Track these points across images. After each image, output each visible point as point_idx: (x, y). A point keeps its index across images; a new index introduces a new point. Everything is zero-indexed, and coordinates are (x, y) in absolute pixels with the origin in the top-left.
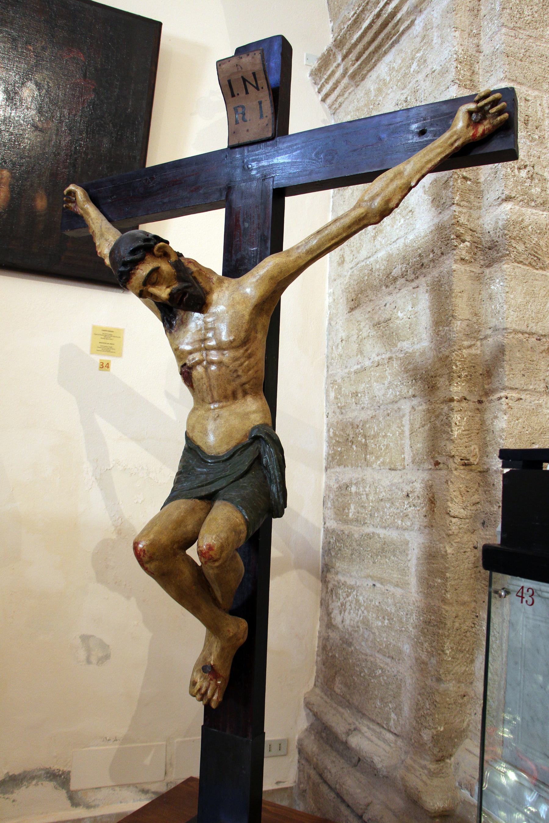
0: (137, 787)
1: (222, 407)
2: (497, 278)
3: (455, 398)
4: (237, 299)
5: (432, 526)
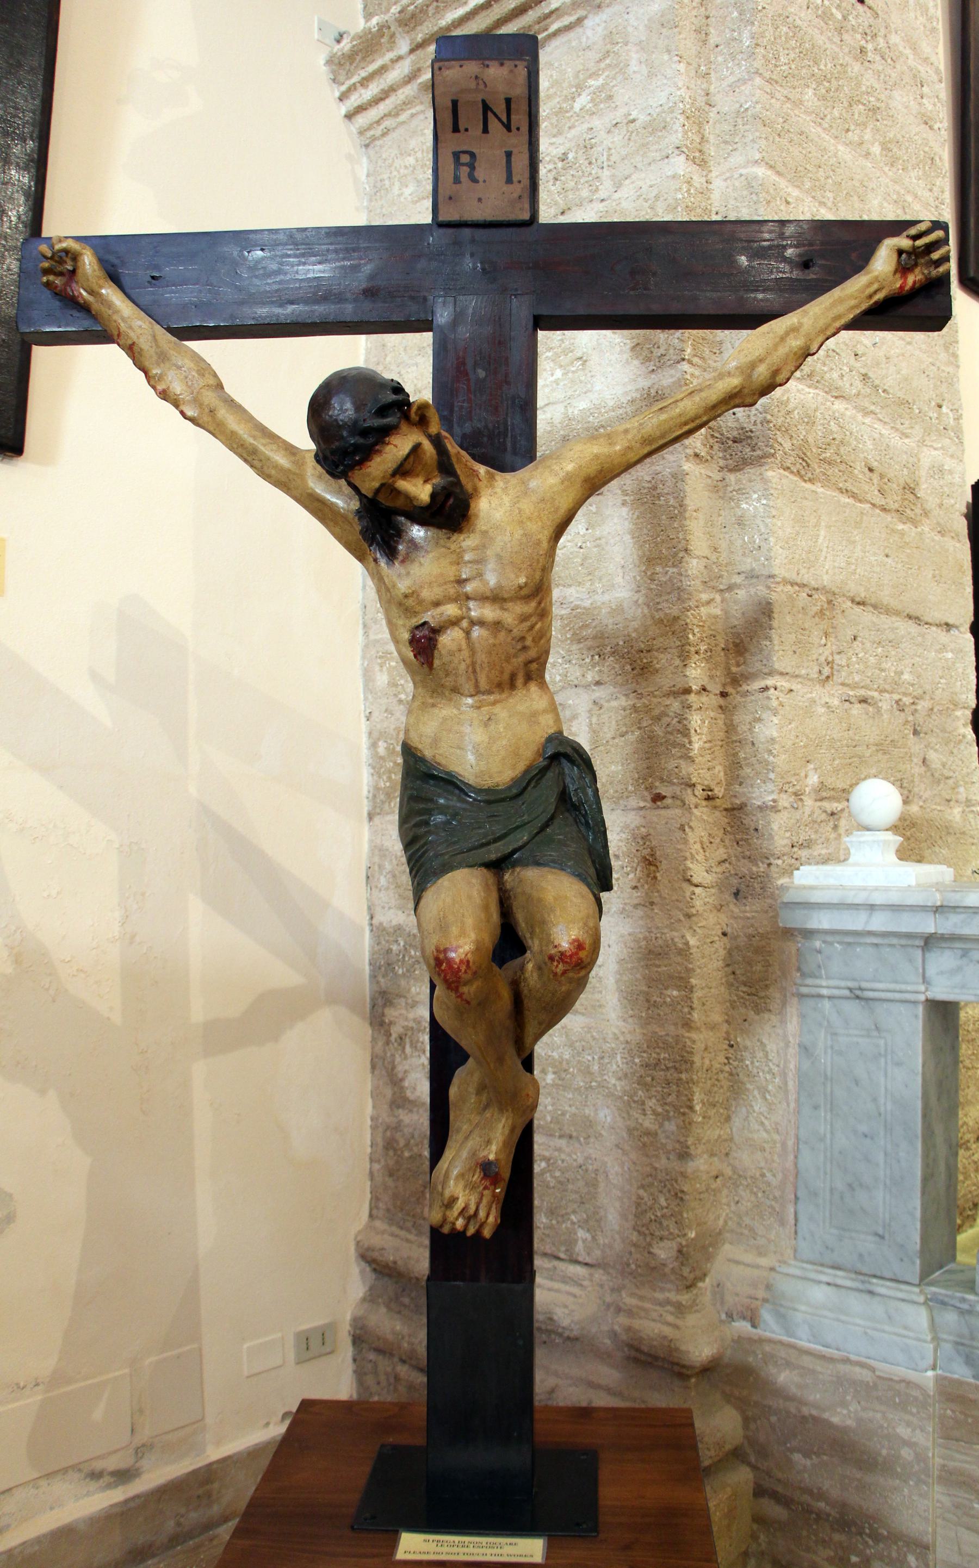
0: (80, 1470)
1: (494, 703)
2: (755, 492)
3: (694, 687)
4: (527, 511)
5: (652, 903)
